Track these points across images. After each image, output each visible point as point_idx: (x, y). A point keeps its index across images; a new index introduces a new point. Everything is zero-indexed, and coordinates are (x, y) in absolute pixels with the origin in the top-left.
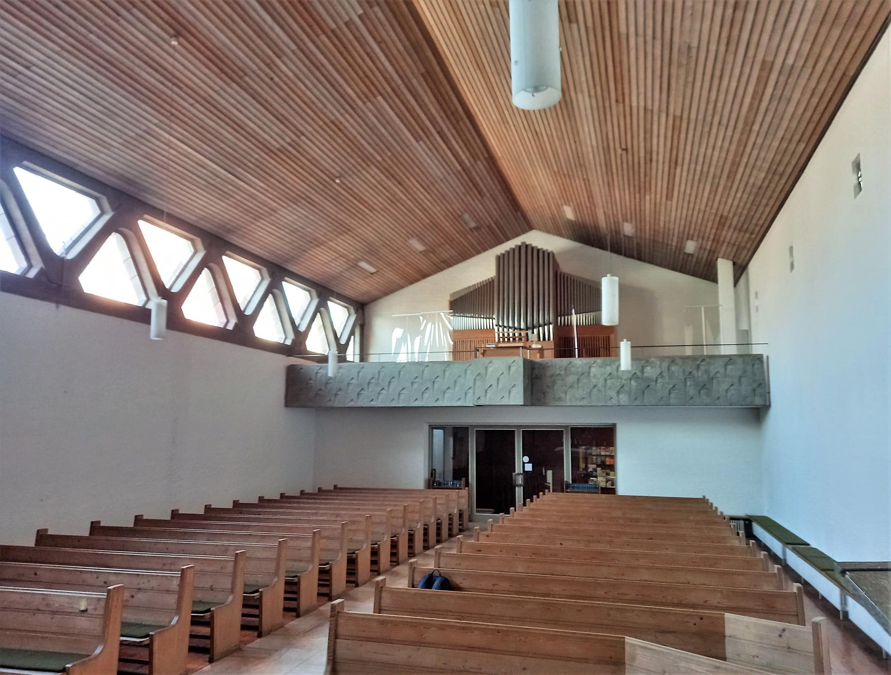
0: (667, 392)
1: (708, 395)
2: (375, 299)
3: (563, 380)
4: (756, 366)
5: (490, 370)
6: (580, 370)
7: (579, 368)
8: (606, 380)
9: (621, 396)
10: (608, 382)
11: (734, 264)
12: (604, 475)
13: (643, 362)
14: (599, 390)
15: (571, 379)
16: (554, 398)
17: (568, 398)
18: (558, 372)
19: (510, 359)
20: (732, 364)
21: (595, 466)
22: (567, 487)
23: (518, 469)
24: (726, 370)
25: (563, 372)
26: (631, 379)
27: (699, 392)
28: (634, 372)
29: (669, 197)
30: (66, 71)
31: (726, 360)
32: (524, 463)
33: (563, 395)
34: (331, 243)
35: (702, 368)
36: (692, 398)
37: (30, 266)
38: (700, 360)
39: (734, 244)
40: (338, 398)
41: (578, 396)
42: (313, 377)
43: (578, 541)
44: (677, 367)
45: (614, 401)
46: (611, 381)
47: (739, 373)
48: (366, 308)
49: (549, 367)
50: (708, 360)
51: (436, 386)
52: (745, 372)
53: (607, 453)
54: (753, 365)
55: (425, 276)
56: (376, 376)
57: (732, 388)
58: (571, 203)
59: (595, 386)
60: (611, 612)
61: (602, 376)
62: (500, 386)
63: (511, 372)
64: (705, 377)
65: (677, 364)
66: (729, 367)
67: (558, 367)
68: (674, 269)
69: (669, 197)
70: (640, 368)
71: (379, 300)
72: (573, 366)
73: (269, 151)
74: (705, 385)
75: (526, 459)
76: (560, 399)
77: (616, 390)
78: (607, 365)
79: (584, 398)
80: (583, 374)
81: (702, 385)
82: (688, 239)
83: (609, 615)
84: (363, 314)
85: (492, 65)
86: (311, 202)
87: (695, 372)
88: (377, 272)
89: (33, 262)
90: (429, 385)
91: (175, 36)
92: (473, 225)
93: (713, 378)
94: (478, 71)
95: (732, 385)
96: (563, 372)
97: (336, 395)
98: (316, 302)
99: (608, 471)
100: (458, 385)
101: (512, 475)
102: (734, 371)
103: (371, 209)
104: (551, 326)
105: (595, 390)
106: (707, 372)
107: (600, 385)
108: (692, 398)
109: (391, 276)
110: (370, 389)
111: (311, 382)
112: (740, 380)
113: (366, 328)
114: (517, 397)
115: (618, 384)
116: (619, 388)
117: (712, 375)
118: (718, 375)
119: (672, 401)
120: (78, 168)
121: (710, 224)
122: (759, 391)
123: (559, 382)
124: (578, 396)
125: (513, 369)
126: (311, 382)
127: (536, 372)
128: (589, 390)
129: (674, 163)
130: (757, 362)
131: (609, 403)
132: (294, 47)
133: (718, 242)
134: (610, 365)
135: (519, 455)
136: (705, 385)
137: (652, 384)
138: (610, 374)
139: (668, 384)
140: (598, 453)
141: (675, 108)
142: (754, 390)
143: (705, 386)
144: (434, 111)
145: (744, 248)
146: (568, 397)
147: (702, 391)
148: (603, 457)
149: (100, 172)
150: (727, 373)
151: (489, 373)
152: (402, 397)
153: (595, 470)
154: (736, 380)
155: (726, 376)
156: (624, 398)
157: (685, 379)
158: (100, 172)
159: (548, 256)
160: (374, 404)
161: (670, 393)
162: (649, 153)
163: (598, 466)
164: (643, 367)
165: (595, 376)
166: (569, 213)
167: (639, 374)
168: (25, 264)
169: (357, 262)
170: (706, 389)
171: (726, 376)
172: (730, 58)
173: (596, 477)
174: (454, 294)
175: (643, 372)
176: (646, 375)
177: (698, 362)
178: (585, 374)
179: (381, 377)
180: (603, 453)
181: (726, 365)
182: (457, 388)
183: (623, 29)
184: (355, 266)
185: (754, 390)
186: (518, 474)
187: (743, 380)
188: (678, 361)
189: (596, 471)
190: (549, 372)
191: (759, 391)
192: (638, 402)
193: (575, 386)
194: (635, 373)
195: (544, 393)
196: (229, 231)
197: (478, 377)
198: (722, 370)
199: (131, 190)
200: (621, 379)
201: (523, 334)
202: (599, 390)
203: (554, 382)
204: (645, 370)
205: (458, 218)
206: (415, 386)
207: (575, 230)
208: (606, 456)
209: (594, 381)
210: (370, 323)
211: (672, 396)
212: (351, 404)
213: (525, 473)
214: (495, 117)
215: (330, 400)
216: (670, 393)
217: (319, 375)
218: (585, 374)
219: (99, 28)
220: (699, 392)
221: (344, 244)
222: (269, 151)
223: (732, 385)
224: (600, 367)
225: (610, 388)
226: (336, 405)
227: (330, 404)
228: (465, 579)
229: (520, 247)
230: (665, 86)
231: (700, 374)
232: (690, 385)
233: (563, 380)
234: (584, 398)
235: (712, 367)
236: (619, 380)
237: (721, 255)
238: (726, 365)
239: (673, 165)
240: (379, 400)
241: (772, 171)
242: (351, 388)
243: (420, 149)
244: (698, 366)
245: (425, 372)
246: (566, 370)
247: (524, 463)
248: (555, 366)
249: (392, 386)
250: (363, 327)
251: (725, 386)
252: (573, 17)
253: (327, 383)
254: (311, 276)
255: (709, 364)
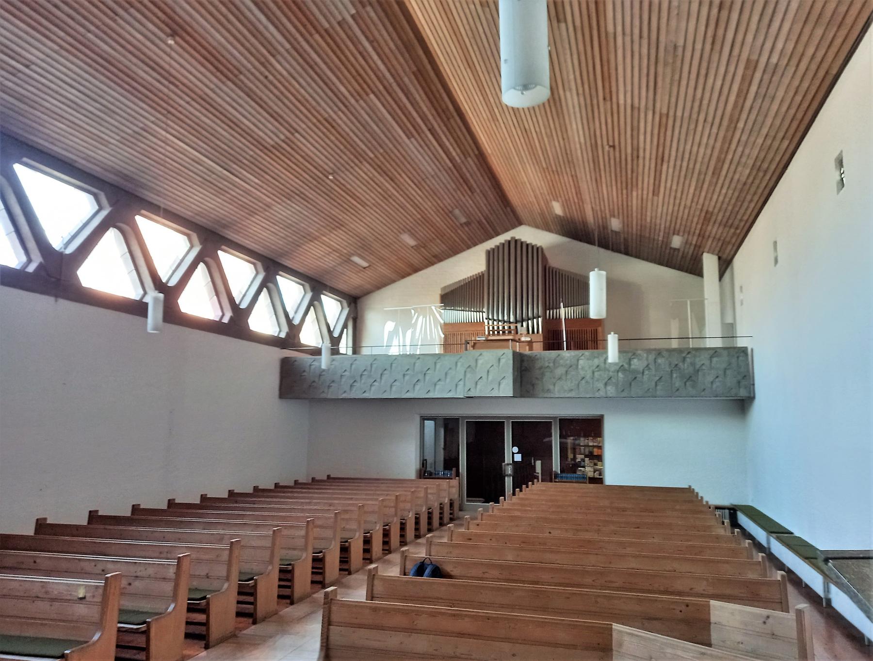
0: (653, 384)
1: (693, 387)
2: (368, 293)
3: (551, 372)
4: (741, 358)
5: (480, 362)
6: (568, 362)
7: (567, 360)
8: (593, 372)
9: (609, 388)
10: (596, 374)
11: (719, 258)
12: (592, 465)
13: (630, 354)
14: (587, 382)
15: (560, 371)
16: (543, 390)
17: (556, 390)
18: (547, 364)
19: (500, 352)
20: (717, 356)
21: (583, 456)
22: (556, 477)
23: (508, 459)
24: (711, 362)
25: (551, 365)
26: (618, 372)
27: (685, 384)
28: (621, 364)
29: (655, 193)
30: (64, 70)
31: (711, 352)
32: (513, 454)
33: (551, 387)
34: (324, 238)
35: (688, 360)
36: (678, 390)
37: (30, 261)
38: (686, 352)
39: (719, 239)
40: (331, 390)
41: (566, 388)
42: (307, 369)
43: (566, 530)
44: (663, 360)
45: (602, 393)
46: (599, 373)
47: (724, 365)
48: (359, 301)
49: (538, 359)
50: (694, 352)
51: (427, 378)
52: (730, 364)
53: (595, 444)
54: (738, 357)
55: (416, 270)
56: (369, 368)
57: (717, 380)
58: (559, 199)
59: (583, 378)
60: (599, 600)
61: (589, 368)
62: (490, 378)
63: (501, 364)
64: (691, 369)
65: (663, 357)
66: (715, 360)
67: (546, 359)
68: (660, 263)
69: (655, 193)
70: (627, 361)
71: (371, 294)
72: (562, 359)
73: (264, 148)
74: (691, 377)
75: (516, 449)
76: (549, 391)
77: (604, 382)
78: (595, 357)
79: (572, 390)
80: (571, 366)
81: (688, 377)
82: (674, 234)
83: (597, 602)
84: (356, 307)
85: (482, 63)
86: (305, 198)
87: (681, 364)
88: (370, 266)
89: (33, 257)
90: (420, 377)
91: (172, 36)
92: (463, 220)
93: (698, 371)
94: (468, 70)
95: (717, 377)
96: (551, 365)
97: (329, 387)
98: (309, 295)
99: (596, 461)
100: (449, 377)
101: (501, 465)
102: (719, 363)
103: (364, 204)
104: (540, 320)
105: (583, 382)
106: (693, 364)
107: (588, 377)
108: (678, 390)
109: (383, 270)
110: (363, 381)
111: (305, 374)
112: (725, 372)
113: (358, 321)
114: (507, 388)
115: (606, 376)
116: (606, 380)
117: (697, 367)
118: (704, 367)
119: (658, 393)
120: (76, 165)
121: (695, 220)
122: (743, 383)
123: (548, 374)
124: (566, 388)
125: (503, 361)
126: (305, 374)
127: (525, 364)
128: (577, 382)
129: (661, 160)
130: (742, 354)
131: (597, 395)
132: (288, 46)
133: (703, 237)
134: (598, 357)
135: (508, 445)
136: (691, 377)
137: (639, 376)
138: (598, 366)
139: (655, 376)
140: (586, 444)
141: (661, 105)
142: (739, 382)
143: (691, 378)
144: (425, 109)
145: (729, 243)
146: (557, 389)
147: (687, 383)
148: (591, 448)
149: (98, 169)
150: (713, 365)
151: (479, 365)
152: (394, 388)
153: (583, 460)
154: (721, 373)
155: (711, 368)
156: (611, 390)
157: (672, 371)
158: (98, 169)
159: (537, 251)
160: (366, 396)
161: (656, 385)
162: (636, 149)
163: (586, 456)
164: (630, 360)
165: (583, 368)
166: (557, 209)
167: (626, 366)
168: (24, 259)
169: (350, 256)
170: (692, 381)
171: (711, 368)
172: (715, 57)
173: (584, 467)
174: (444, 288)
175: (630, 364)
176: (633, 367)
177: (684, 355)
178: (574, 366)
179: (373, 369)
180: (591, 444)
181: (711, 357)
182: (448, 380)
183: (610, 28)
184: (348, 260)
185: (739, 382)
186: (508, 464)
187: (728, 372)
188: (665, 353)
189: (584, 461)
190: (538, 364)
191: (743, 383)
192: (625, 394)
193: (564, 378)
194: (622, 366)
195: (533, 385)
196: (225, 226)
197: (469, 370)
198: (707, 362)
199: (129, 186)
200: (609, 371)
201: (513, 327)
202: (587, 382)
203: (543, 374)
204: (632, 362)
205: (448, 213)
206: (407, 378)
207: (563, 225)
208: (594, 446)
209: (582, 373)
210: (362, 317)
211: (658, 387)
212: (344, 396)
213: (515, 463)
214: (485, 114)
215: (323, 392)
216: (656, 385)
217: (313, 367)
218: (574, 366)
219: (97, 27)
220: (685, 384)
221: (337, 239)
222: (264, 148)
223: (717, 377)
224: (588, 359)
225: (598, 380)
226: (329, 396)
227: (323, 396)
228: (456, 567)
229: (509, 242)
230: (652, 84)
231: (686, 367)
232: (676, 377)
233: (551, 372)
234: (572, 390)
235: (697, 360)
236: (607, 372)
237: (706, 249)
238: (711, 357)
239: (659, 162)
240: (372, 392)
241: (757, 168)
242: (344, 380)
243: (411, 146)
244: (684, 359)
245: (417, 365)
246: (554, 362)
247: (513, 454)
248: (544, 358)
249: (384, 378)
250: (355, 320)
251: (710, 378)
252: (561, 17)
253: (320, 375)
254: (305, 270)
255: (695, 356)
